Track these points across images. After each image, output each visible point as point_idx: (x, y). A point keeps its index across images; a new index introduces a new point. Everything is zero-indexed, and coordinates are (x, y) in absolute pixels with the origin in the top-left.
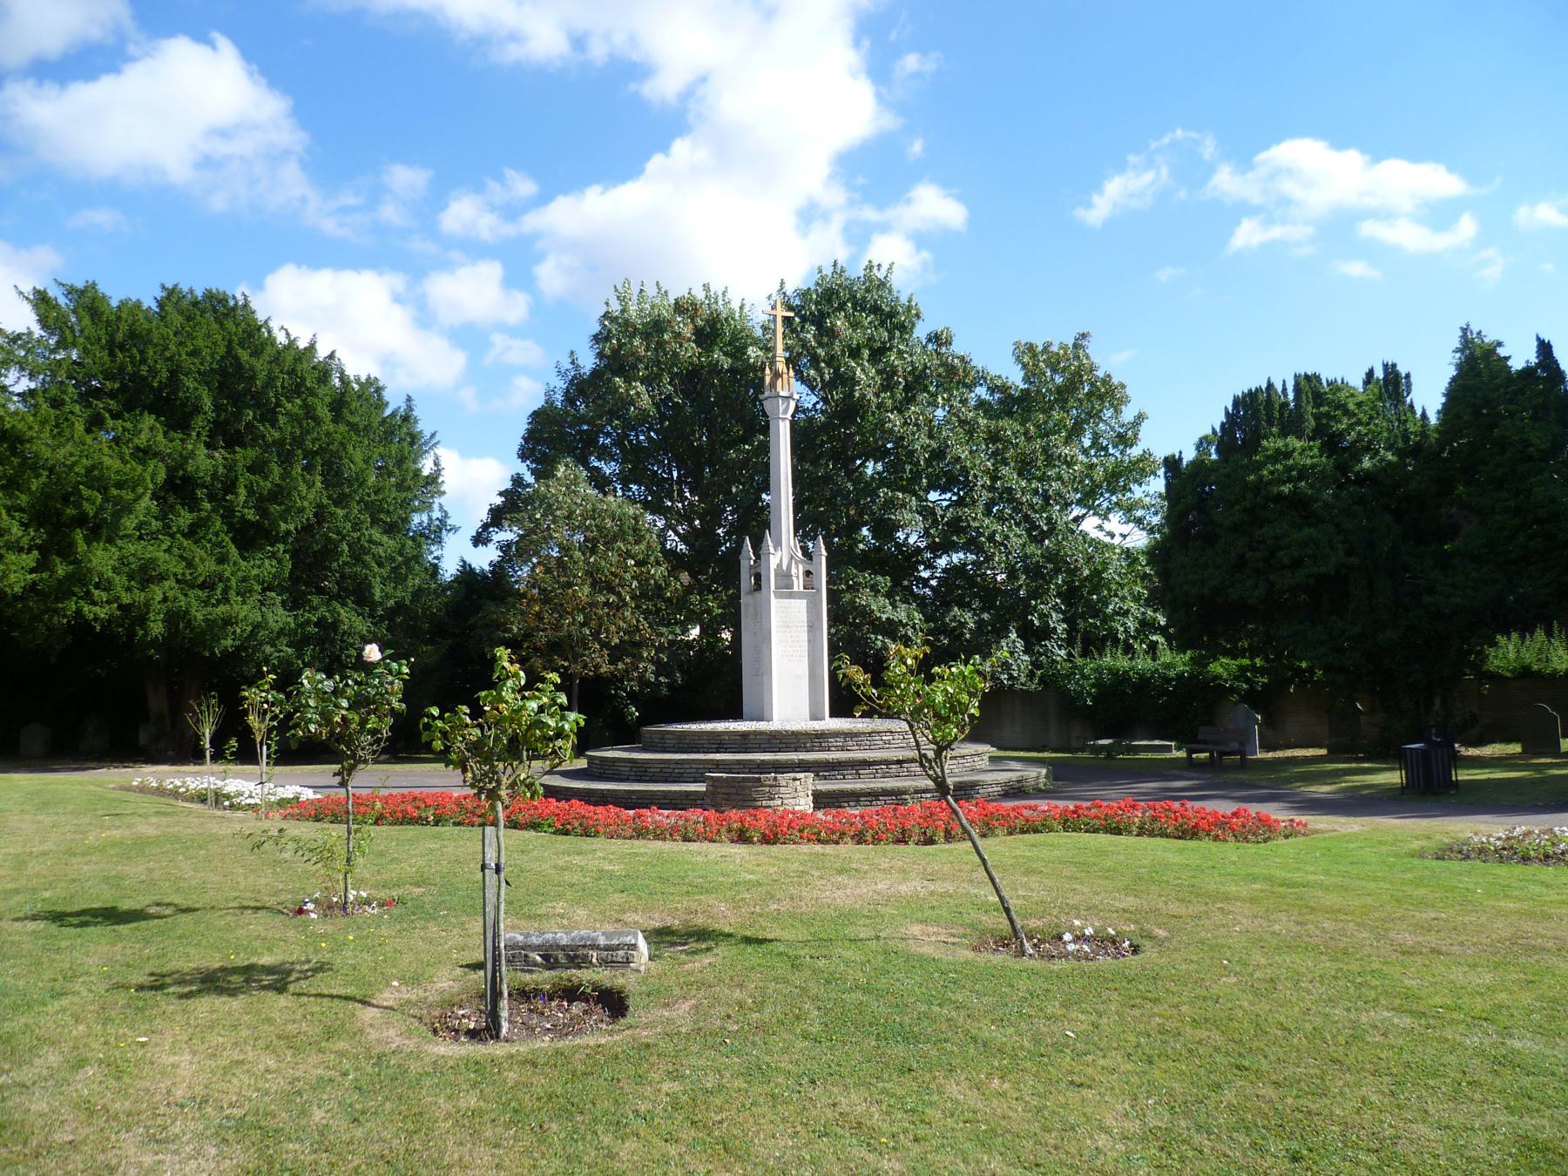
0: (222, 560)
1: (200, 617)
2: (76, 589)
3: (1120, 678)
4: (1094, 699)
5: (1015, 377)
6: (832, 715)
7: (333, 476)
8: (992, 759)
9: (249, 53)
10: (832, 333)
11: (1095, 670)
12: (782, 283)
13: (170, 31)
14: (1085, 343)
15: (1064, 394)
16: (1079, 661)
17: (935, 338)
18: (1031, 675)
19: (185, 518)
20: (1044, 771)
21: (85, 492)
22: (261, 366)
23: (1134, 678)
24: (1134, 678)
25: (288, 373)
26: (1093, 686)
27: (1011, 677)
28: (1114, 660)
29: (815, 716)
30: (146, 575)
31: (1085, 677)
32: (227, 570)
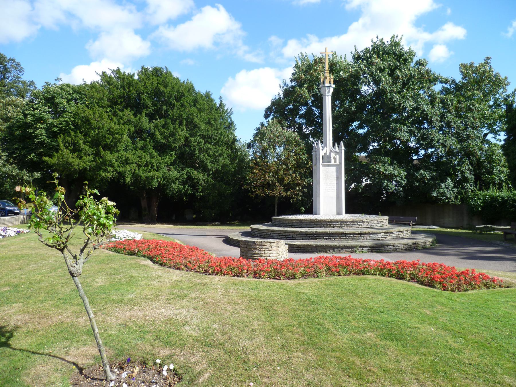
0: (152, 157)
1: (143, 176)
2: (103, 167)
3: (494, 199)
4: (482, 208)
5: (458, 78)
6: (347, 212)
7: (192, 126)
8: (413, 232)
9: (229, 10)
10: (372, 64)
11: (483, 196)
12: (355, 47)
13: (204, 5)
14: (489, 61)
15: (478, 83)
16: (477, 192)
17: (419, 63)
18: (456, 198)
19: (141, 144)
20: (430, 240)
21: (108, 136)
22: (167, 91)
23: (500, 199)
24: (500, 199)
25: (177, 92)
26: (482, 203)
27: (447, 198)
28: (493, 192)
29: (339, 213)
30: (126, 162)
31: (479, 199)
32: (153, 161)
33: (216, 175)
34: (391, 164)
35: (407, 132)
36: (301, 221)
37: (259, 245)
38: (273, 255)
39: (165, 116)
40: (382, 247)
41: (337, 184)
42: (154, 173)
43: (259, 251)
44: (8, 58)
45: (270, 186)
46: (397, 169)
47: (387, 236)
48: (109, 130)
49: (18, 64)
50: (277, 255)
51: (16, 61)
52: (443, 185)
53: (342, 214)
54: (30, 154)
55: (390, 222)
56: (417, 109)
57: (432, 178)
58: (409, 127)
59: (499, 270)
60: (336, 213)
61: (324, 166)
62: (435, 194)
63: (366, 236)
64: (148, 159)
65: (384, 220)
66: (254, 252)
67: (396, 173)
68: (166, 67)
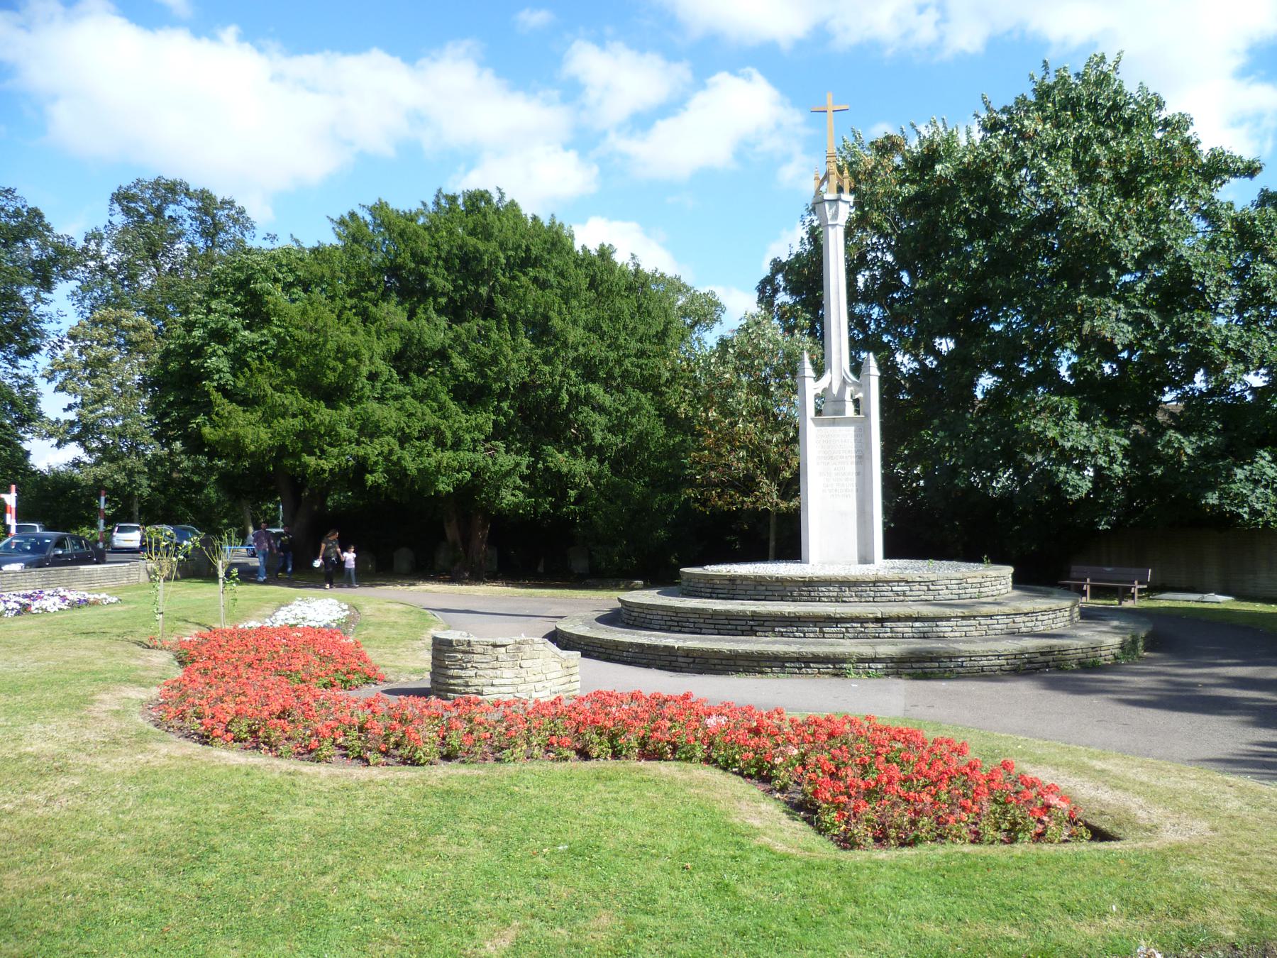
6: (890, 553)
29: (865, 559)
33: (621, 461)
34: (1082, 417)
35: (1125, 321)
36: (733, 579)
37: (464, 652)
38: (502, 681)
39: (489, 311)
40: (932, 660)
41: (858, 474)
42: (446, 456)
43: (462, 669)
44: (219, 200)
45: (747, 485)
46: (1101, 430)
47: (971, 627)
48: (339, 350)
49: (241, 212)
50: (517, 681)
51: (237, 205)
52: (1239, 474)
53: (872, 562)
54: (195, 417)
55: (1019, 581)
56: (1157, 253)
57: (1205, 454)
58: (1135, 307)
59: (1123, 752)
60: (856, 559)
61: (818, 424)
62: (1212, 498)
63: (901, 627)
64: (432, 420)
65: (997, 578)
66: (451, 672)
67: (1094, 444)
68: (499, 190)
